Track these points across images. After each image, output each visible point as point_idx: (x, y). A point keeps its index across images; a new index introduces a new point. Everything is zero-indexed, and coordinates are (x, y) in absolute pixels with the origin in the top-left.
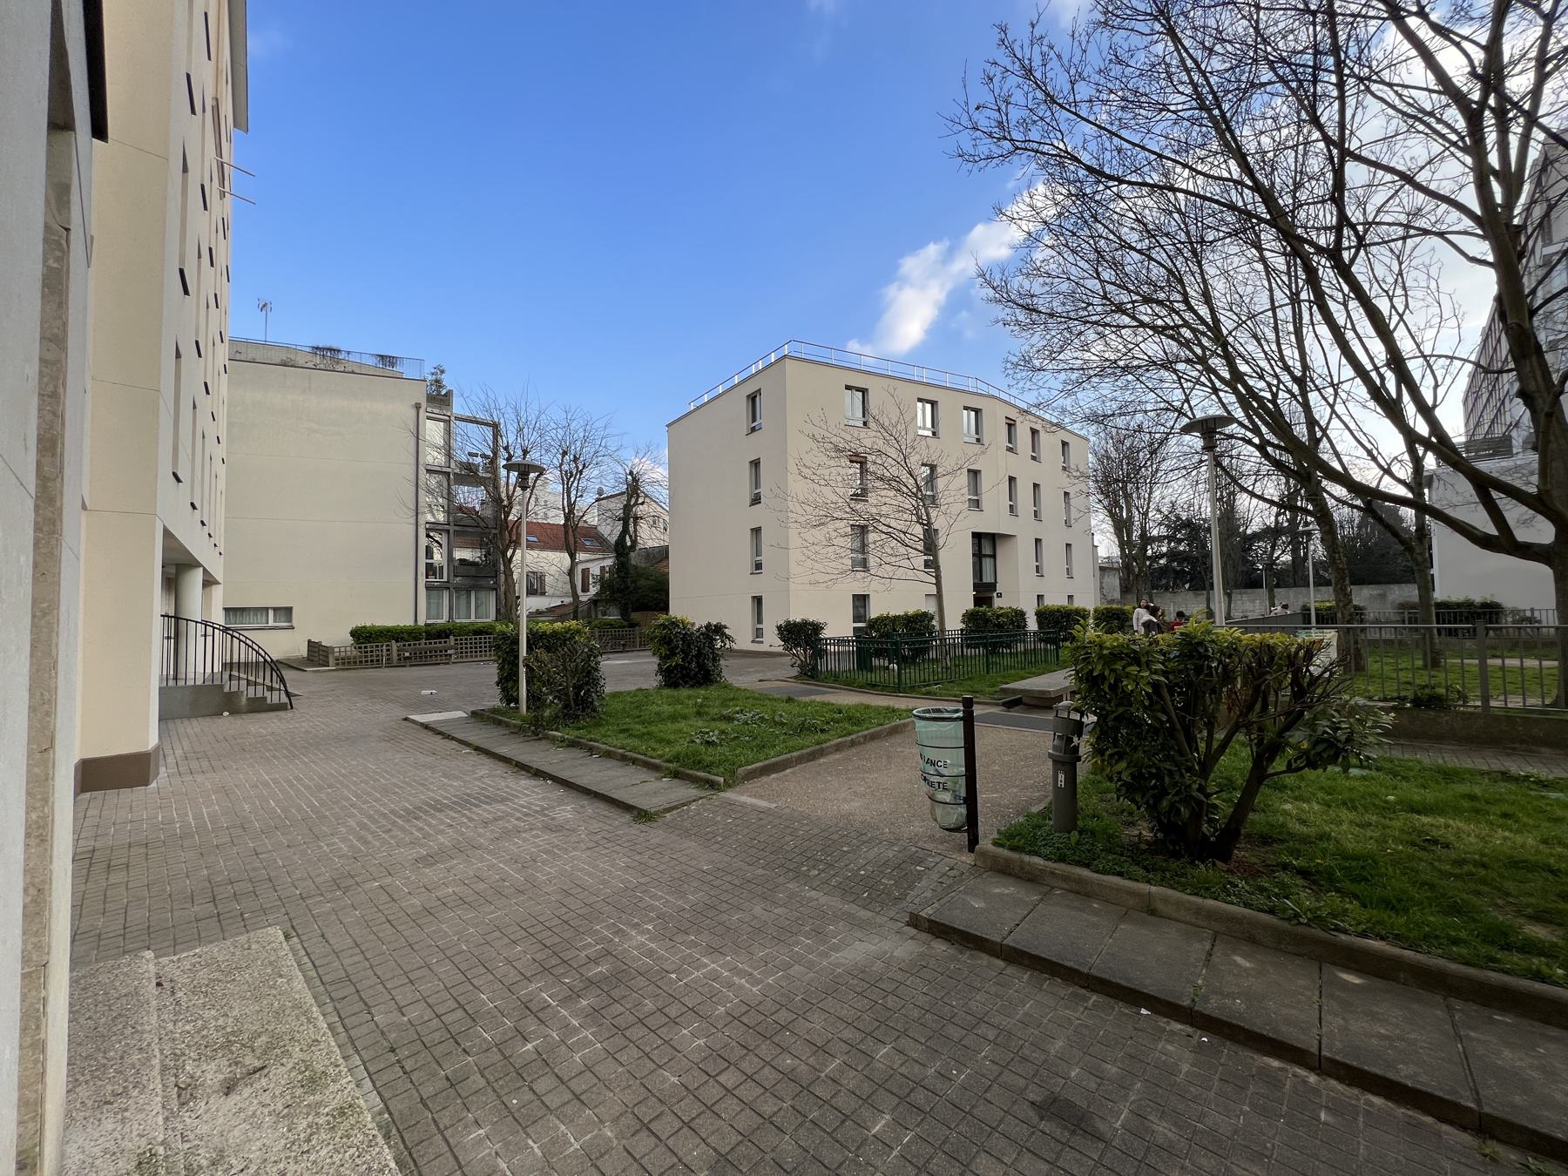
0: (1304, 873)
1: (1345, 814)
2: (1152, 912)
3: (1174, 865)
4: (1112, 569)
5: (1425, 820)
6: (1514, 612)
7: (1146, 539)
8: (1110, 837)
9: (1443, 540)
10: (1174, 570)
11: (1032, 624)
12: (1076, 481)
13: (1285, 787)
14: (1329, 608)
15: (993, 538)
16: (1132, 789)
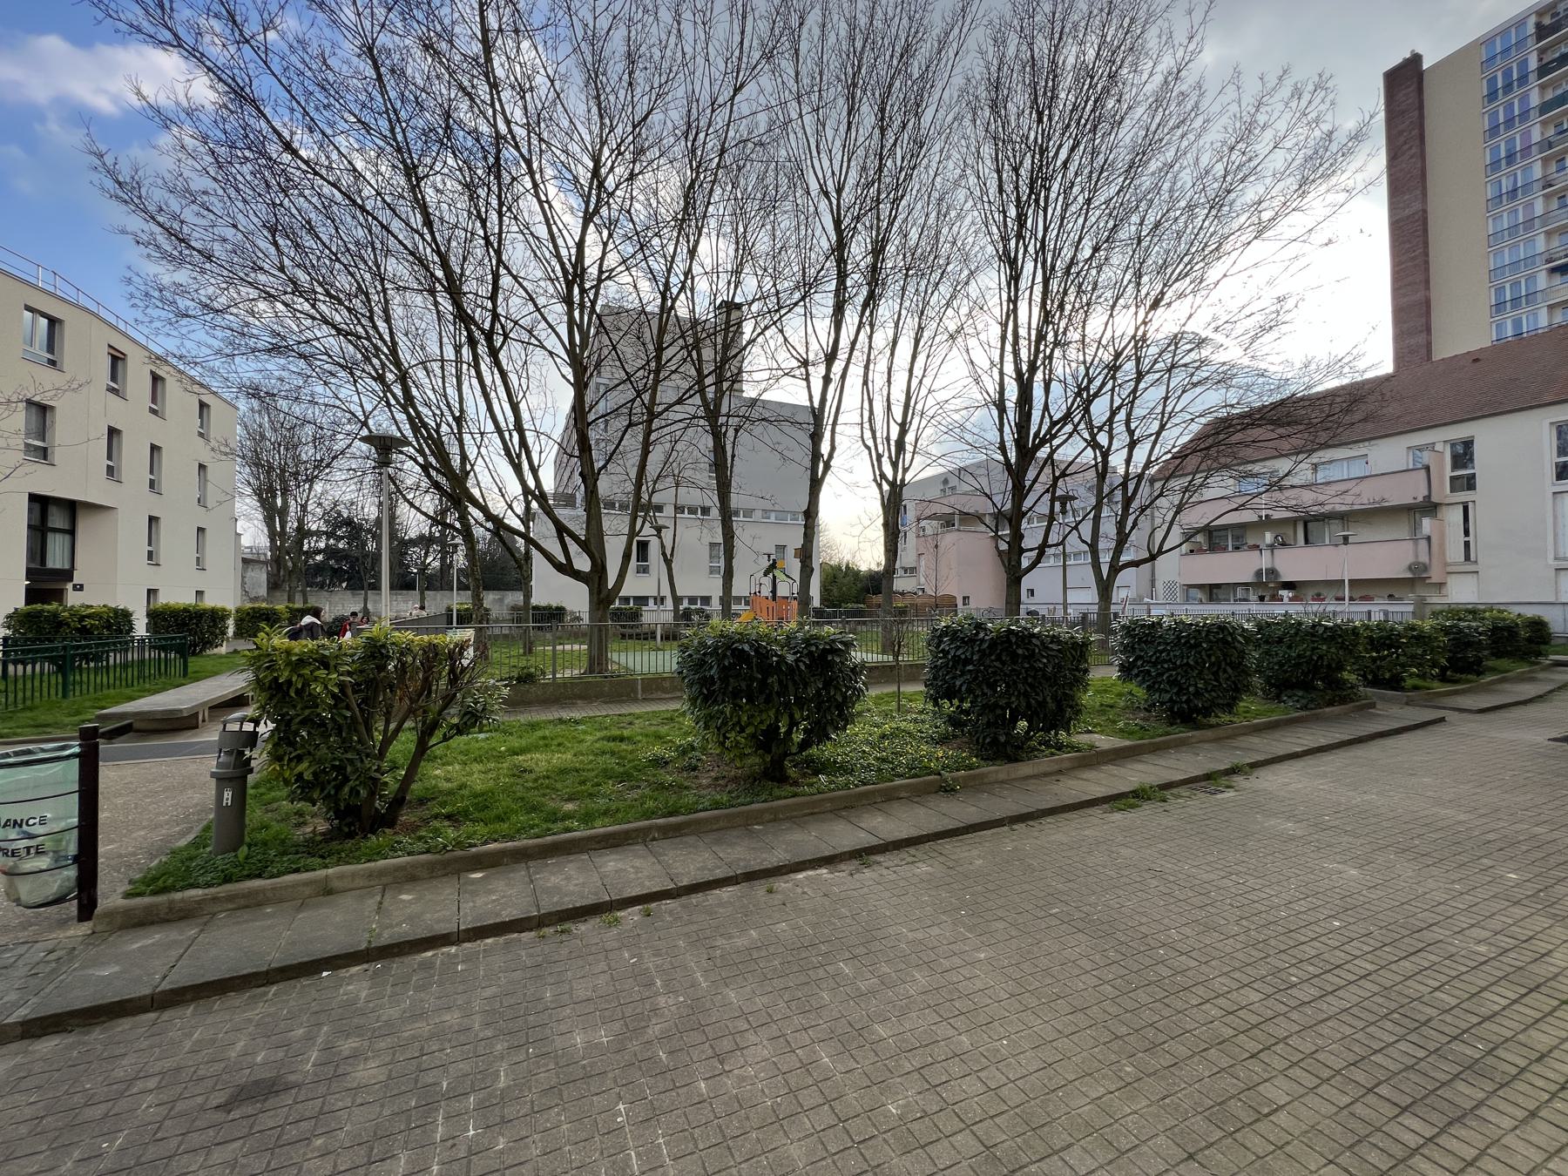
0: (449, 817)
1: (476, 767)
2: (329, 892)
3: (349, 844)
4: (258, 562)
5: (520, 758)
6: (572, 613)
7: (303, 533)
8: (283, 842)
9: (539, 563)
10: (332, 568)
11: (140, 628)
12: (224, 457)
13: (436, 757)
14: (467, 609)
15: (72, 508)
16: (304, 789)
